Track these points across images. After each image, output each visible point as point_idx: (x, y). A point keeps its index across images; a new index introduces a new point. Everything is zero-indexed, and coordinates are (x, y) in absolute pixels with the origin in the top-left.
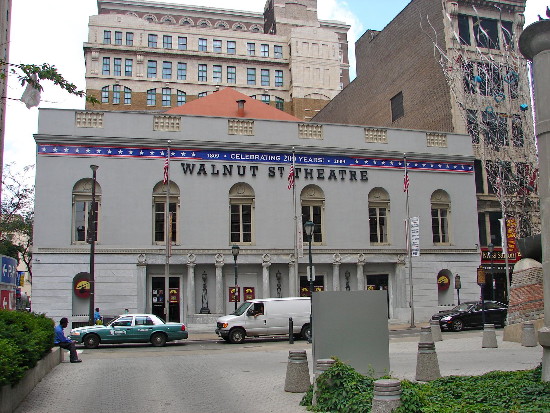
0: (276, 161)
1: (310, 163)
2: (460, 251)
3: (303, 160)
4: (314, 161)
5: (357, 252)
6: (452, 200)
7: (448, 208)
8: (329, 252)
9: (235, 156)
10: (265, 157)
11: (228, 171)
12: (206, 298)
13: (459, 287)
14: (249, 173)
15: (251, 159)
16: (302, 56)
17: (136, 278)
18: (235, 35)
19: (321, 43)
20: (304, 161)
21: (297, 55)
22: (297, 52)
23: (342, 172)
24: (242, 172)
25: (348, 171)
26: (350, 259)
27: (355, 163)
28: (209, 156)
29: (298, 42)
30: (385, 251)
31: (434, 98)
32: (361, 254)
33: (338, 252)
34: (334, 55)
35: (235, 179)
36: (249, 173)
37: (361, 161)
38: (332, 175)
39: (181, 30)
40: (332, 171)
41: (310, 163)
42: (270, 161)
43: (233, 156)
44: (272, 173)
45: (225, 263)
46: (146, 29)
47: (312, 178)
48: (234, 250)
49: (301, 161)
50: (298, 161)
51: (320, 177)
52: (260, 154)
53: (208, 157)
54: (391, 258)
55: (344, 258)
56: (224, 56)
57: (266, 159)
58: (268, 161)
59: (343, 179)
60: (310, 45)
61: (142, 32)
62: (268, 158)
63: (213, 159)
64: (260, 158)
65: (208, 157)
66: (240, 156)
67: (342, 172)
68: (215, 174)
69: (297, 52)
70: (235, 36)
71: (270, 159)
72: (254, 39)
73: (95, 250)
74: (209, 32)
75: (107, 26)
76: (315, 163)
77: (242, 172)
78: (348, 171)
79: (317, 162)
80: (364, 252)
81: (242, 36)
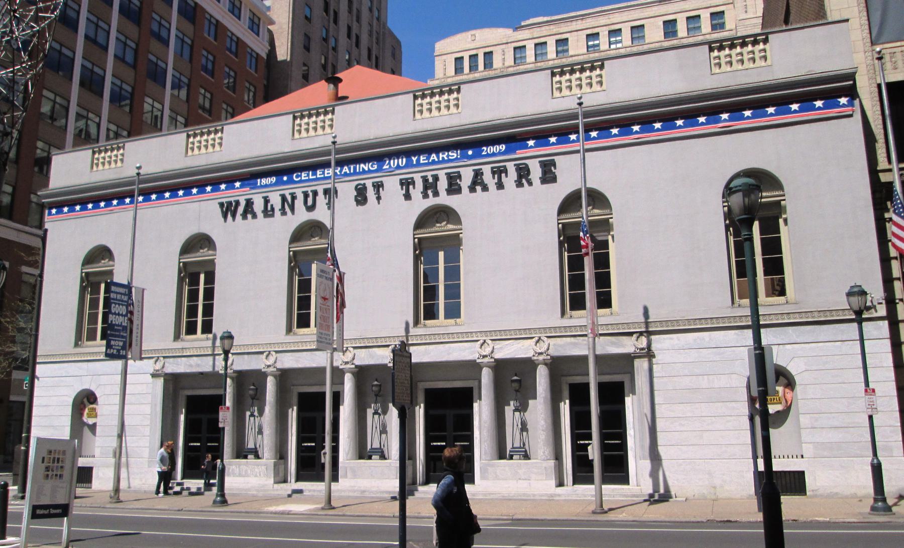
0: (370, 171)
1: (434, 162)
2: (816, 314)
3: (418, 160)
4: (441, 159)
5: (531, 334)
8: (466, 338)
9: (301, 176)
10: (350, 169)
11: (288, 204)
14: (321, 200)
15: (326, 175)
16: (755, 16)
17: (150, 396)
18: (642, 14)
20: (422, 162)
21: (745, 17)
23: (499, 172)
24: (310, 202)
25: (511, 167)
26: (515, 351)
28: (261, 182)
32: (540, 338)
33: (487, 336)
35: (302, 215)
36: (321, 200)
37: (541, 137)
38: (477, 181)
39: (559, 29)
40: (478, 174)
41: (434, 162)
42: (360, 173)
43: (297, 177)
44: (361, 197)
45: (235, 369)
46: (509, 41)
47: (436, 194)
48: (855, 300)
49: (415, 163)
50: (409, 165)
51: (454, 188)
52: (408, 153)
53: (259, 184)
54: (613, 344)
55: (501, 348)
56: (626, 50)
57: (352, 172)
58: (355, 173)
59: (500, 186)
61: (504, 46)
62: (355, 169)
63: (266, 186)
64: (341, 171)
67: (499, 172)
68: (268, 212)
69: (746, 12)
70: (642, 15)
71: (358, 171)
72: (673, 12)
74: (601, 21)
75: (458, 50)
76: (444, 161)
77: (310, 202)
78: (511, 167)
79: (446, 158)
80: (546, 333)
81: (654, 12)
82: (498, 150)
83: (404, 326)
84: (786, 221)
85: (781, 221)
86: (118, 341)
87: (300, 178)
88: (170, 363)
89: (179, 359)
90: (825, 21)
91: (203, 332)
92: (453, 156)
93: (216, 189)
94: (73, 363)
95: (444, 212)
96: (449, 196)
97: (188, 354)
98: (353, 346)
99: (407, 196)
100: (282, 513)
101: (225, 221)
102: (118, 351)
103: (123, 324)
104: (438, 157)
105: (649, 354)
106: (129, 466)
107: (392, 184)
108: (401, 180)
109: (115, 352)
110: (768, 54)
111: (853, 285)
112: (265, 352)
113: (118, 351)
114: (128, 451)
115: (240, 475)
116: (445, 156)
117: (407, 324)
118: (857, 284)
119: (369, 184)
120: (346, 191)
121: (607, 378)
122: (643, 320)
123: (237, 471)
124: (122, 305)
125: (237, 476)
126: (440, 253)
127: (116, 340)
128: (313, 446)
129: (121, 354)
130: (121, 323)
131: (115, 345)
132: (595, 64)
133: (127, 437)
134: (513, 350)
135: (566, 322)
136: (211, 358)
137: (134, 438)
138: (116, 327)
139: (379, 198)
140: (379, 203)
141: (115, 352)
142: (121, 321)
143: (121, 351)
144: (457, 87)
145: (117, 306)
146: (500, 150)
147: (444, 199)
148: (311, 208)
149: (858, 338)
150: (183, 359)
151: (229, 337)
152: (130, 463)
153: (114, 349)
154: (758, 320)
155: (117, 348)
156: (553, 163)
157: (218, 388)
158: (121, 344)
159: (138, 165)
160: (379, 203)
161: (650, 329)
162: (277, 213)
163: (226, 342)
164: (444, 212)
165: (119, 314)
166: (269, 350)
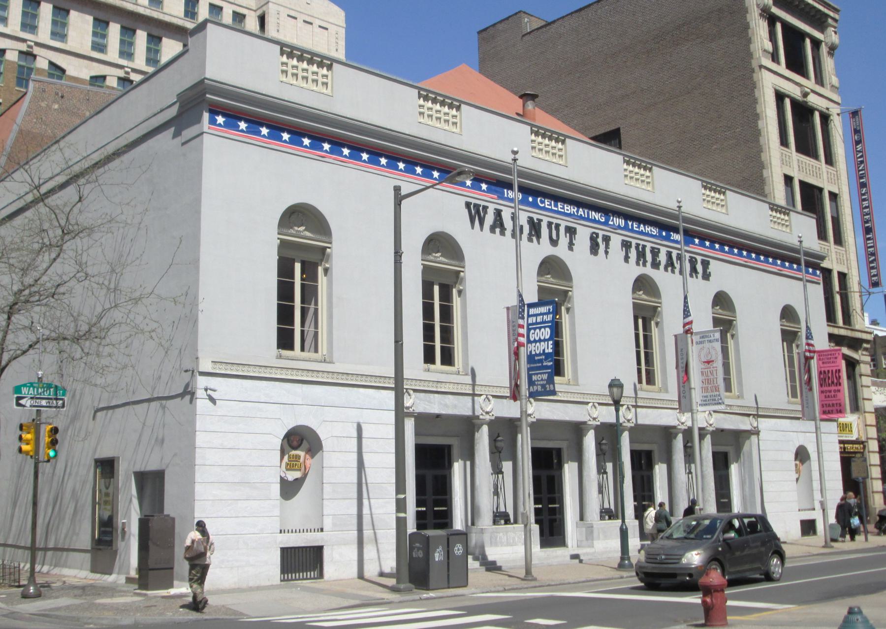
12: (503, 489)
13: (865, 475)
14: (564, 240)
19: (317, 22)
22: (278, 31)
27: (694, 243)
29: (280, 13)
30: (737, 408)
31: (715, 147)
34: (337, 50)
36: (564, 240)
43: (542, 202)
52: (579, 204)
56: (145, 11)
60: (300, 22)
65: (506, 196)
66: (550, 205)
69: (278, 31)
73: (405, 382)
83: (633, 387)
85: (320, 269)
86: (541, 373)
87: (543, 205)
89: (432, 396)
91: (443, 362)
92: (654, 232)
93: (476, 186)
94: (277, 383)
95: (432, 240)
96: (653, 270)
97: (443, 390)
98: (414, 388)
99: (627, 259)
100: (666, 568)
101: (473, 227)
102: (543, 386)
103: (547, 351)
104: (577, 211)
105: (757, 433)
106: (379, 541)
107: (616, 241)
108: (623, 241)
109: (539, 388)
111: (614, 378)
112: (590, 402)
113: (543, 386)
114: (374, 520)
115: (508, 544)
116: (649, 229)
117: (635, 385)
119: (649, 246)
120: (583, 234)
121: (639, 447)
122: (634, 396)
123: (504, 539)
124: (545, 327)
125: (505, 546)
126: (435, 286)
127: (537, 374)
128: (424, 511)
129: (548, 389)
130: (544, 350)
131: (538, 380)
132: (315, 58)
133: (372, 501)
136: (469, 398)
137: (381, 501)
138: (536, 358)
139: (607, 253)
140: (607, 258)
141: (539, 388)
142: (542, 348)
143: (547, 386)
144: (329, 63)
145: (538, 330)
147: (648, 270)
149: (394, 409)
150: (436, 395)
152: (378, 536)
153: (537, 385)
155: (542, 383)
156: (708, 263)
157: (448, 436)
158: (545, 377)
159: (515, 149)
160: (607, 258)
161: (760, 413)
162: (662, 267)
163: (615, 390)
164: (432, 240)
165: (540, 341)
166: (628, 403)
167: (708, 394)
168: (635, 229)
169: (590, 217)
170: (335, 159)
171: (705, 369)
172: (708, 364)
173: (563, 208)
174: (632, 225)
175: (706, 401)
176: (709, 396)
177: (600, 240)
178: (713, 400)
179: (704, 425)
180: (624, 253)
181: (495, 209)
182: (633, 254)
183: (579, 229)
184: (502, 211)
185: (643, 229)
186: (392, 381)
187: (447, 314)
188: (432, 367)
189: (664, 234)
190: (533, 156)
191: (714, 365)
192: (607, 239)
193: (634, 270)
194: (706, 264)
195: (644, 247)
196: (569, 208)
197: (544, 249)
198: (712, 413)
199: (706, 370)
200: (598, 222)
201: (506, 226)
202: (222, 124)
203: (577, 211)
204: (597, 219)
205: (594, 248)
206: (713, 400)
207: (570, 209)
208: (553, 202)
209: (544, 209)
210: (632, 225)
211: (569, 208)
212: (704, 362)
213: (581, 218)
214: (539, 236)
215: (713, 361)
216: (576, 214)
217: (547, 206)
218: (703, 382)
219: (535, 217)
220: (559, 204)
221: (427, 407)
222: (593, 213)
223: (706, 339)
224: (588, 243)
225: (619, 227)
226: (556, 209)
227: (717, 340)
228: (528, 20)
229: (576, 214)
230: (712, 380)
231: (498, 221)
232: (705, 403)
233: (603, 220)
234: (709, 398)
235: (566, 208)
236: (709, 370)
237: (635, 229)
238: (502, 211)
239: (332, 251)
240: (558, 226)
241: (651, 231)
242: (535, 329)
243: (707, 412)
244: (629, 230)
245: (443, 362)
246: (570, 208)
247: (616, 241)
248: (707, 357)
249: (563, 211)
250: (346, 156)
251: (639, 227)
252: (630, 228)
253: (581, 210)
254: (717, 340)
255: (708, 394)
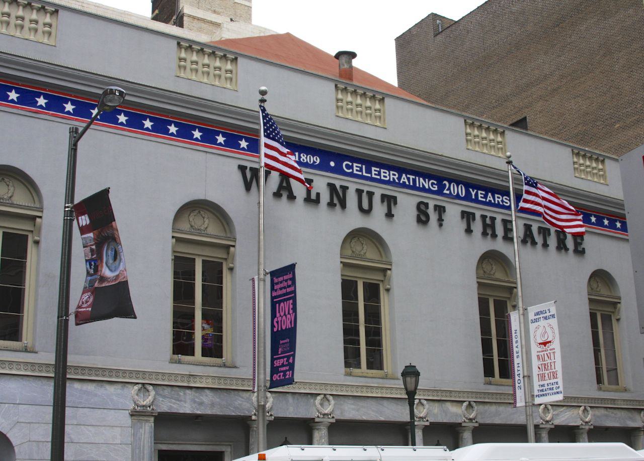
2: (210, 380)
6: (395, 255)
7: (613, 312)
10: (408, 179)
36: (379, 209)
43: (348, 167)
52: (401, 170)
66: (361, 170)
82: (312, 162)
84: (37, 243)
87: (351, 171)
88: (164, 397)
90: (351, 83)
91: (370, 366)
99: (469, 231)
104: (399, 179)
107: (453, 211)
110: (53, 31)
112: (319, 394)
116: (500, 200)
118: (412, 365)
134: (566, 417)
135: (492, 389)
146: (314, 162)
147: (499, 245)
148: (366, 212)
151: (411, 372)
154: (65, 373)
163: (410, 380)
166: (470, 400)
167: (545, 382)
168: (480, 199)
169: (418, 185)
170: (53, 115)
171: (542, 351)
172: (545, 346)
173: (379, 174)
174: (476, 195)
175: (542, 391)
176: (546, 385)
177: (431, 211)
178: (550, 389)
179: (538, 421)
180: (464, 226)
181: (525, 225)
182: (477, 227)
183: (401, 198)
184: (531, 226)
185: (492, 199)
186: (52, 369)
187: (374, 316)
188: (356, 371)
189: (332, 164)
190: (576, 177)
191: (551, 347)
192: (440, 210)
193: (480, 245)
194: (578, 237)
195: (493, 219)
196: (387, 175)
197: (353, 219)
198: (550, 407)
199: (542, 353)
200: (429, 191)
201: (568, 247)
202: (246, 148)
203: (399, 179)
204: (427, 187)
205: (422, 218)
206: (550, 389)
207: (385, 174)
208: (364, 166)
209: (352, 175)
210: (476, 195)
211: (387, 175)
212: (540, 344)
213: (404, 185)
214: (343, 205)
215: (550, 342)
216: (397, 181)
217: (355, 172)
218: (539, 368)
219: (338, 184)
220: (373, 169)
221: (175, 406)
222: (421, 180)
223: (541, 316)
224: (414, 212)
225: (458, 197)
226: (369, 175)
227: (553, 316)
228: (440, 22)
229: (397, 181)
230: (549, 365)
231: (284, 188)
232: (542, 393)
233: (436, 189)
234: (546, 387)
235: (382, 174)
236: (545, 353)
237: (480, 199)
238: (531, 226)
239: (235, 250)
240: (370, 194)
241: (502, 201)
242: (279, 302)
243: (582, 408)
244: (472, 200)
245: (370, 366)
246: (389, 175)
247: (453, 211)
248: (543, 336)
249: (379, 177)
250: (197, 138)
251: (485, 197)
252: (473, 197)
253: (404, 176)
254: (553, 316)
255: (545, 382)
